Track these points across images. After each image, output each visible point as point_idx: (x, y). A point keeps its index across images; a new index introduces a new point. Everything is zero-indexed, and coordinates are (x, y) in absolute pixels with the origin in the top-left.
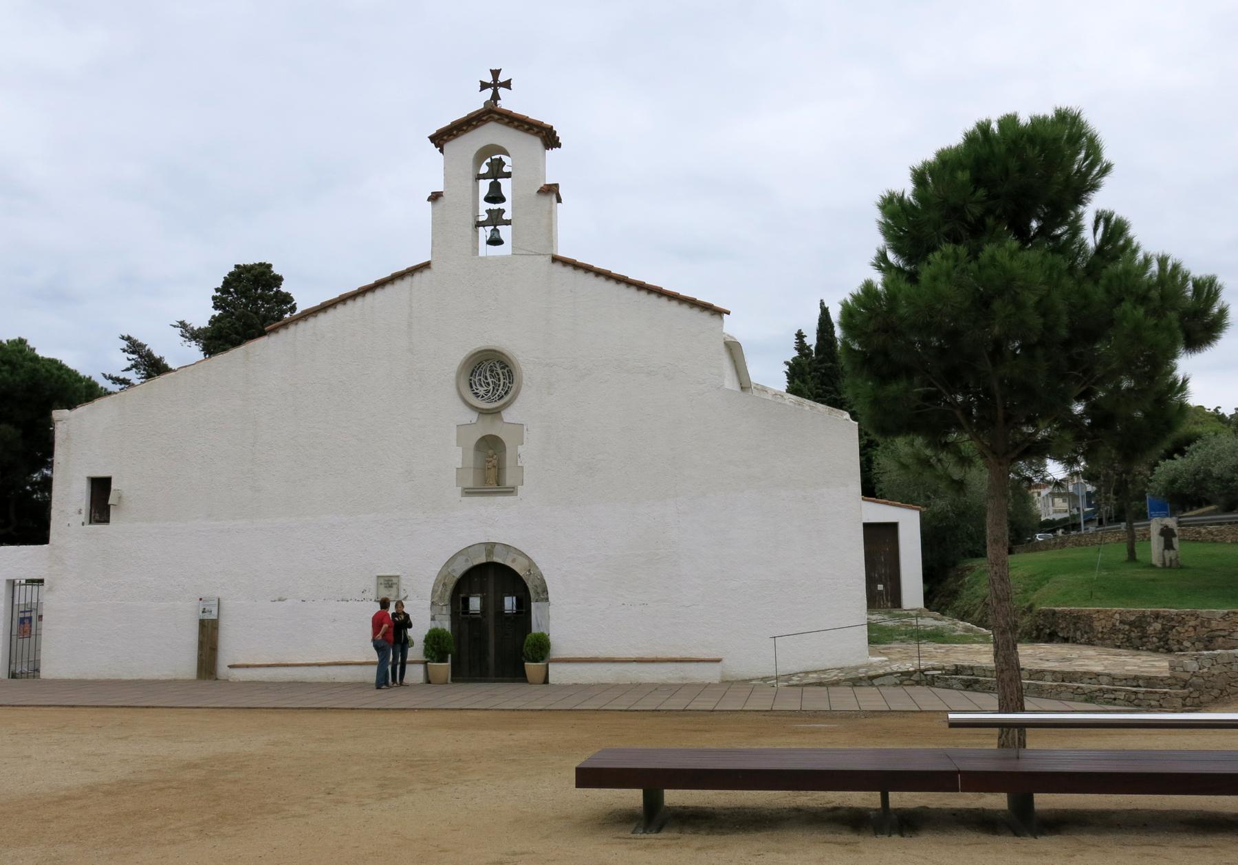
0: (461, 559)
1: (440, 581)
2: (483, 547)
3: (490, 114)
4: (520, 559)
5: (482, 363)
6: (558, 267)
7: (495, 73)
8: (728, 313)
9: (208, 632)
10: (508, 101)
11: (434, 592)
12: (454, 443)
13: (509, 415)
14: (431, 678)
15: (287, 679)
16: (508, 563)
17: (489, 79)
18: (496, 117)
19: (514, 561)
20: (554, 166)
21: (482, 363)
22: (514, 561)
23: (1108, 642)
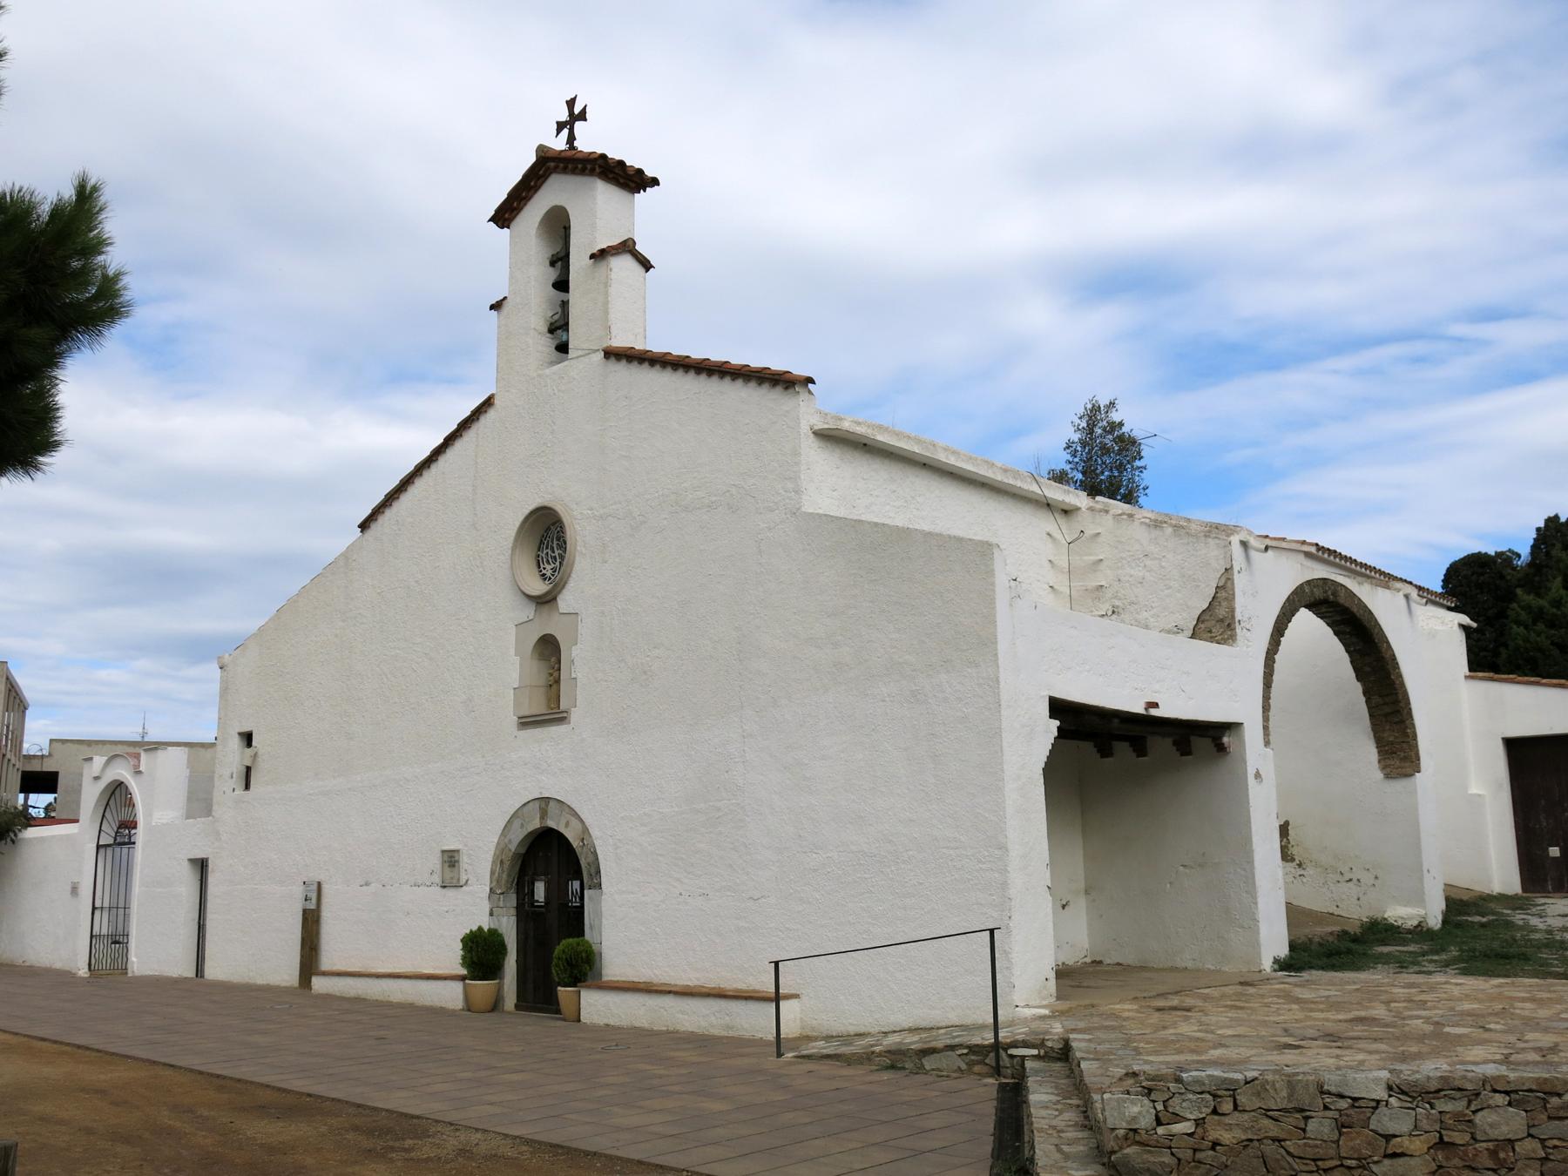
0: (517, 823)
1: (499, 860)
2: (537, 804)
3: (547, 166)
4: (574, 822)
5: (548, 529)
6: (621, 370)
7: (571, 104)
8: (813, 382)
9: (311, 922)
10: (589, 140)
11: (492, 873)
12: (512, 651)
13: (566, 601)
14: (1294, 851)
15: (352, 993)
16: (562, 830)
17: (564, 117)
18: (552, 164)
19: (567, 825)
20: (644, 217)
21: (548, 529)
22: (567, 825)
23: (1279, 1099)
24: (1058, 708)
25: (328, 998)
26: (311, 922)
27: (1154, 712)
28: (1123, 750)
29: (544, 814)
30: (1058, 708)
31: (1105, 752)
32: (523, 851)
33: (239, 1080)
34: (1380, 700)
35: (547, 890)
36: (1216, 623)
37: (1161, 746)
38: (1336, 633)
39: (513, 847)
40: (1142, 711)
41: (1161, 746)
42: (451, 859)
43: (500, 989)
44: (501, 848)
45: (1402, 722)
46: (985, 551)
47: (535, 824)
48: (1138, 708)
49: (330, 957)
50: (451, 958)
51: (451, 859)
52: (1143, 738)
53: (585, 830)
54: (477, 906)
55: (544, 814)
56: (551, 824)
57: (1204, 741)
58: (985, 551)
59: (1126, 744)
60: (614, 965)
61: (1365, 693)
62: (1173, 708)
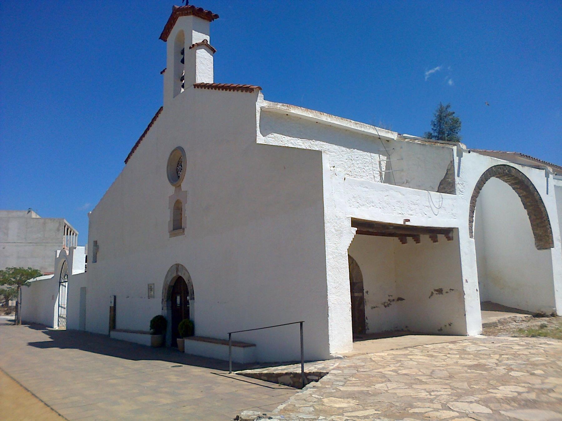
9: (113, 310)
19: (184, 274)
22: (184, 274)
24: (355, 222)
25: (117, 341)
26: (113, 310)
27: (407, 223)
28: (410, 239)
29: (177, 271)
30: (355, 222)
31: (403, 241)
32: (173, 284)
33: (211, 342)
34: (535, 217)
35: (181, 299)
36: (447, 186)
37: (425, 238)
38: (514, 189)
39: (168, 283)
40: (402, 223)
41: (425, 238)
42: (151, 288)
43: (164, 338)
44: (165, 284)
45: (545, 226)
46: (318, 154)
47: (174, 275)
48: (401, 222)
49: (119, 325)
50: (147, 327)
51: (151, 288)
52: (418, 235)
53: (190, 277)
54: (157, 307)
55: (177, 271)
56: (180, 274)
57: (449, 233)
58: (318, 154)
59: (411, 238)
60: (199, 330)
61: (528, 214)
62: (415, 222)
